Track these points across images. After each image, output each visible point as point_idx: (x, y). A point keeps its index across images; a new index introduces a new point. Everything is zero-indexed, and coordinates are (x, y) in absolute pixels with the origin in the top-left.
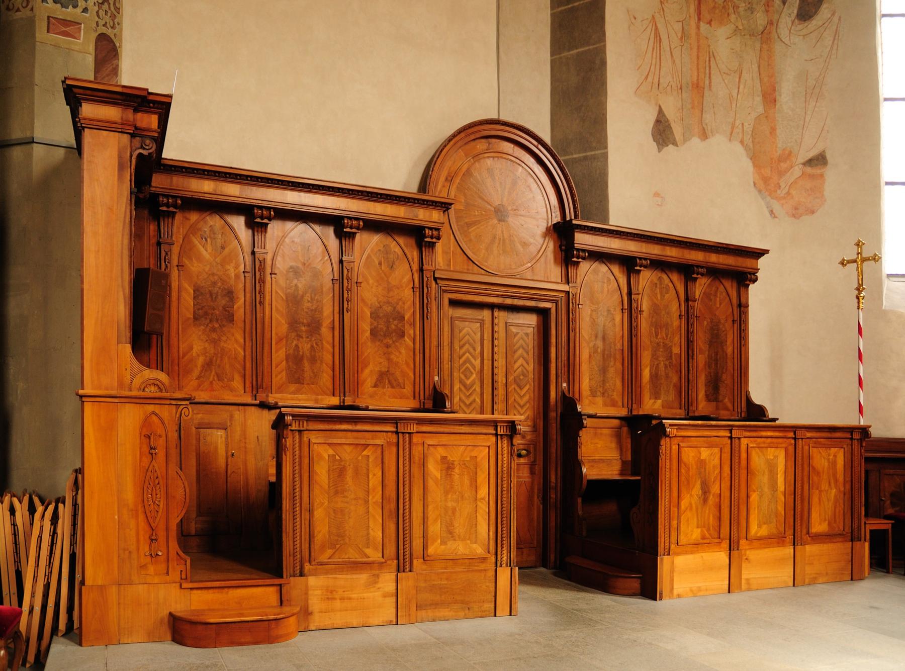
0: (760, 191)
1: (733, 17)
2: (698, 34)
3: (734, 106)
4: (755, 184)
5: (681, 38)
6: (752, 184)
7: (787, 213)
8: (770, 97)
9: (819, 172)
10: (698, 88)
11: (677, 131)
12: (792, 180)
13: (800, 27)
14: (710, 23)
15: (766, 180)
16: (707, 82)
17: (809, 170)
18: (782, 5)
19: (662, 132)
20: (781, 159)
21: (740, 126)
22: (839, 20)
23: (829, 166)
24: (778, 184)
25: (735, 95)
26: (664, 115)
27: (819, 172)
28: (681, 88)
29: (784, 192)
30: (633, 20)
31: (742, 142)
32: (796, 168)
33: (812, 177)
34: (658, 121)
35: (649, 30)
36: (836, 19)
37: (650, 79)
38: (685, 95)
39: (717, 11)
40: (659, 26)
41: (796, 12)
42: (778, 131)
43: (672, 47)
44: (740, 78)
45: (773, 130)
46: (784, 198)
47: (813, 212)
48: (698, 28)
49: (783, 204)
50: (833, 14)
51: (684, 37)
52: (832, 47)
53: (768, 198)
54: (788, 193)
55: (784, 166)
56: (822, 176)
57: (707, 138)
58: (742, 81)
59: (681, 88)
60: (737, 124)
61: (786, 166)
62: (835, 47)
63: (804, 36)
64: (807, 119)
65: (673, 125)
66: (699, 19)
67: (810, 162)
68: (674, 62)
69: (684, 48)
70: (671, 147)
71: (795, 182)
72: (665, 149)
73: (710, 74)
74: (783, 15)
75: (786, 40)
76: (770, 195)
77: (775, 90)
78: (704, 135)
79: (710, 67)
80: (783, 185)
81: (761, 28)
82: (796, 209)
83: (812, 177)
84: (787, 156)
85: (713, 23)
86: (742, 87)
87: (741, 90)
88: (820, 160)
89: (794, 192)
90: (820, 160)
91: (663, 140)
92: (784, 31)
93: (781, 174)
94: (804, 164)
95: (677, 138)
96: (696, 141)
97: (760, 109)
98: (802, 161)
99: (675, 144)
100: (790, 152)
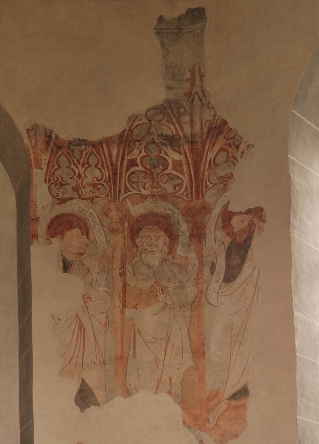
0: (189, 427)
1: (161, 297)
2: (123, 319)
3: (160, 366)
4: (184, 423)
5: (106, 324)
6: (182, 423)
7: (215, 441)
8: (199, 352)
9: (242, 402)
10: (122, 359)
11: (99, 395)
12: (219, 414)
13: (227, 288)
14: (136, 307)
15: (195, 418)
16: (131, 353)
17: (233, 403)
18: (211, 275)
19: (85, 398)
20: (208, 399)
21: (168, 380)
22: (259, 272)
23: (250, 396)
24: (208, 419)
25: (161, 356)
26: (86, 385)
27: (242, 402)
28: (104, 363)
29: (212, 424)
30: (57, 322)
31: (169, 392)
32: (223, 403)
33: (236, 408)
34: (81, 391)
35: (73, 326)
36: (256, 273)
37: (74, 361)
38: (108, 367)
39: (144, 296)
40: (83, 320)
41: (222, 277)
42: (206, 378)
43: (96, 333)
44: (167, 343)
45: (202, 378)
46: (213, 429)
47: (237, 436)
48: (123, 313)
49: (211, 434)
50: (254, 270)
51: (108, 323)
52: (253, 297)
53: (198, 432)
54: (216, 425)
55: (212, 404)
56: (244, 405)
57: (131, 395)
58: (170, 344)
59: (104, 363)
60: (164, 378)
61: (213, 403)
62: (256, 297)
63: (229, 295)
64: (232, 362)
65: (95, 391)
66: (124, 306)
67: (234, 396)
68: (97, 344)
69: (107, 332)
70: (93, 408)
71: (222, 415)
72: (87, 410)
73: (134, 346)
74: (212, 283)
75: (214, 303)
76: (199, 429)
77: (204, 345)
78: (127, 393)
79: (135, 341)
80: (211, 419)
81: (192, 299)
82: (223, 436)
83: (236, 408)
84: (215, 395)
85: (139, 306)
86: (169, 349)
87: (168, 352)
88: (243, 392)
89: (221, 423)
90: (243, 392)
91: (86, 404)
92: (212, 296)
93: (209, 410)
94: (229, 399)
95: (99, 400)
96: (119, 400)
97: (190, 363)
98: (228, 396)
99: (97, 404)
100: (218, 391)
